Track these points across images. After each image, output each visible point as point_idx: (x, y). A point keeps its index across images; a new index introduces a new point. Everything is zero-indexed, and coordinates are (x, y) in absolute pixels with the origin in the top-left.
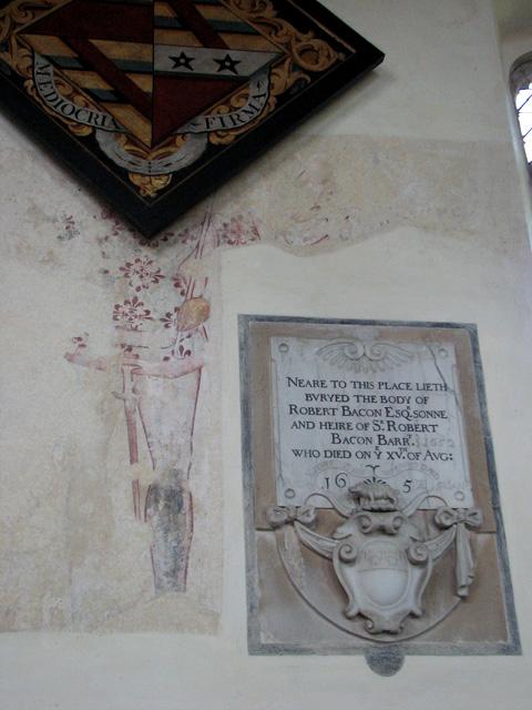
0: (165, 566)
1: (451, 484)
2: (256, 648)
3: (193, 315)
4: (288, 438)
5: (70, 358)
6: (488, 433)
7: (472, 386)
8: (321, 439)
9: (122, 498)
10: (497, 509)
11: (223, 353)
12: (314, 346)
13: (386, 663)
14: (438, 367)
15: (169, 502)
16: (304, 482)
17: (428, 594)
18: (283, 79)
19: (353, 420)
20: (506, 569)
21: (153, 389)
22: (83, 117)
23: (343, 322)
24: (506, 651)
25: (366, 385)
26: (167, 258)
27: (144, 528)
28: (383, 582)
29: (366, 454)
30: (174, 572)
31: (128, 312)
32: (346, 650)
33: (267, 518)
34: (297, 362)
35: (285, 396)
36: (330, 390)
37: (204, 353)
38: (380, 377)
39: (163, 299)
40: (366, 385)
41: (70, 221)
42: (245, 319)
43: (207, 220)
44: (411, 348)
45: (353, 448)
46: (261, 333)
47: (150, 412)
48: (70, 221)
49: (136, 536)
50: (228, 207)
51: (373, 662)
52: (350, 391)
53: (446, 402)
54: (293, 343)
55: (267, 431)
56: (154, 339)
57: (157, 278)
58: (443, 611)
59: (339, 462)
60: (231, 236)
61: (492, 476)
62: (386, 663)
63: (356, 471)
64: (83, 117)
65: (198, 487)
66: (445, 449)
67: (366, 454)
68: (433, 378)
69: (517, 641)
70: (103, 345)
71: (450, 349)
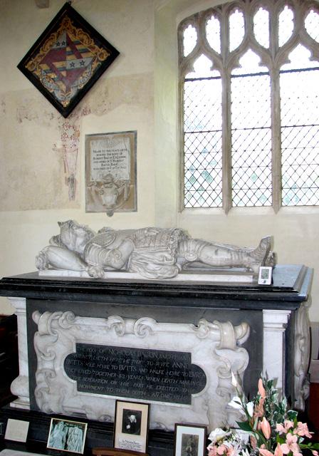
0: (71, 195)
1: (125, 174)
2: (87, 212)
3: (76, 136)
4: (93, 165)
5: (53, 149)
6: (136, 160)
7: (134, 148)
8: (99, 165)
9: (63, 181)
10: (136, 179)
11: (83, 139)
12: (99, 141)
13: (110, 214)
14: (125, 145)
15: (72, 181)
16: (96, 176)
17: (117, 202)
18: (95, 65)
19: (106, 160)
20: (136, 193)
21: (69, 155)
22: (52, 87)
23: (107, 134)
24: (134, 211)
25: (109, 151)
26: (71, 121)
27: (67, 187)
28: (109, 198)
29: (108, 168)
30: (72, 197)
31: (64, 136)
32: (103, 212)
33: (89, 183)
34: (97, 146)
35: (93, 155)
36: (102, 153)
37: (78, 146)
38: (113, 148)
39: (70, 132)
40: (109, 151)
41: (52, 114)
42: (87, 135)
43: (80, 109)
44: (120, 140)
45: (106, 167)
46: (91, 138)
47: (68, 161)
48: (52, 114)
49: (66, 189)
50: (84, 104)
51: (108, 214)
52: (106, 153)
53: (126, 154)
54: (95, 142)
55: (90, 164)
56: (69, 142)
57: (70, 127)
58: (121, 203)
59: (102, 171)
60: (85, 113)
61: (136, 170)
62: (110, 214)
63: (106, 172)
64: (52, 87)
65: (77, 177)
66: (125, 166)
67: (108, 168)
68: (124, 148)
69: (137, 209)
70: (59, 146)
71: (128, 139)
